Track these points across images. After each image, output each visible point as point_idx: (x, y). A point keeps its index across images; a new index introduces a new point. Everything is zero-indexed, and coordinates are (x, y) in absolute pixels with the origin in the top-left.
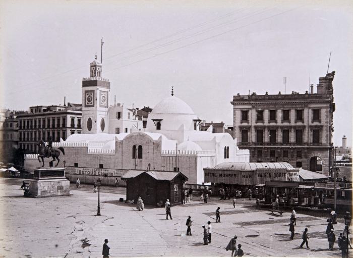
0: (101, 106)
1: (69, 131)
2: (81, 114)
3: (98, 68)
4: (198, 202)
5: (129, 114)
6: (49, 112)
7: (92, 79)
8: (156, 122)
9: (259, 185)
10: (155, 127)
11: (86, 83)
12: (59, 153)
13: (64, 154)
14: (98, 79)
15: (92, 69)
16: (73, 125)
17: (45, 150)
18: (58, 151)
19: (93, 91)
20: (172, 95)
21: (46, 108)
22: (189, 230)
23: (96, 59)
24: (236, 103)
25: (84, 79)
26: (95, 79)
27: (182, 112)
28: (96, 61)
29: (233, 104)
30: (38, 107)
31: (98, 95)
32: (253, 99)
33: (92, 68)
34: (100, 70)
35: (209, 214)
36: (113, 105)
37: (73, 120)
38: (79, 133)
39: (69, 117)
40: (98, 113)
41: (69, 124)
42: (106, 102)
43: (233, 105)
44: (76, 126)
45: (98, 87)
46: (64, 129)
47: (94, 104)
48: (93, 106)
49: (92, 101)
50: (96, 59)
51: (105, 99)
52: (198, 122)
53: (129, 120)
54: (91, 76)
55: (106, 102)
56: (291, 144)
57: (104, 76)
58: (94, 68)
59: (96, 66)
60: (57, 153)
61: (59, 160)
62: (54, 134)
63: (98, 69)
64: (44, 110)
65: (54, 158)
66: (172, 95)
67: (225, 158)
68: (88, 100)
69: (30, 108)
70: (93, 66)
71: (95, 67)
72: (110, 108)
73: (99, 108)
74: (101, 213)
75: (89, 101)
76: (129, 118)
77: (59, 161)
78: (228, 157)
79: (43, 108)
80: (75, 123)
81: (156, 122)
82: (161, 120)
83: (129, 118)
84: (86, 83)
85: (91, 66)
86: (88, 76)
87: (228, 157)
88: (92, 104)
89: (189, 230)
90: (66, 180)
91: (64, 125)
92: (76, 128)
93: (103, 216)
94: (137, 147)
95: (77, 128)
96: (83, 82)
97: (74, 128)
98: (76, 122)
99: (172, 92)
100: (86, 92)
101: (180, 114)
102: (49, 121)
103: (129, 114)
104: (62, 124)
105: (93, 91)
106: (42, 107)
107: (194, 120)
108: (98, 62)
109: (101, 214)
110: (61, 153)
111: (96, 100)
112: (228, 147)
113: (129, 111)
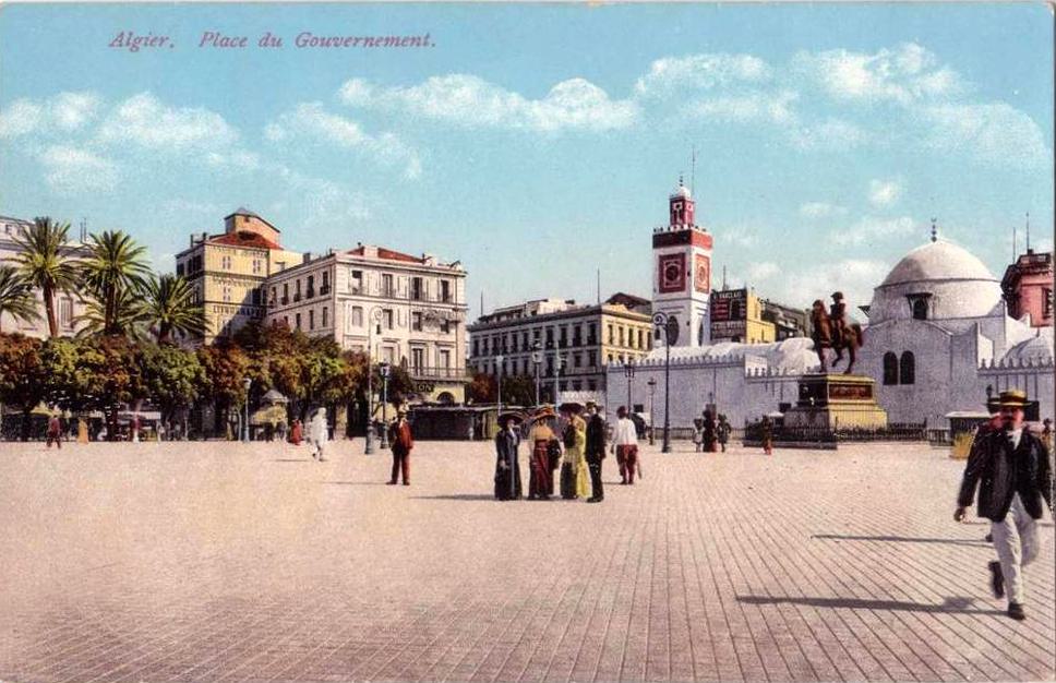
0: (699, 289)
4: (645, 316)
11: (660, 240)
19: (682, 256)
22: (415, 41)
31: (694, 265)
32: (515, 499)
33: (675, 205)
39: (605, 319)
47: (684, 284)
48: (682, 288)
54: (674, 222)
56: (1021, 373)
57: (700, 222)
58: (678, 207)
65: (839, 352)
68: (668, 277)
69: (227, 219)
70: (676, 201)
71: (681, 203)
75: (670, 278)
84: (660, 240)
86: (664, 222)
89: (415, 41)
96: (655, 237)
100: (662, 258)
101: (951, 280)
104: (574, 340)
111: (689, 274)
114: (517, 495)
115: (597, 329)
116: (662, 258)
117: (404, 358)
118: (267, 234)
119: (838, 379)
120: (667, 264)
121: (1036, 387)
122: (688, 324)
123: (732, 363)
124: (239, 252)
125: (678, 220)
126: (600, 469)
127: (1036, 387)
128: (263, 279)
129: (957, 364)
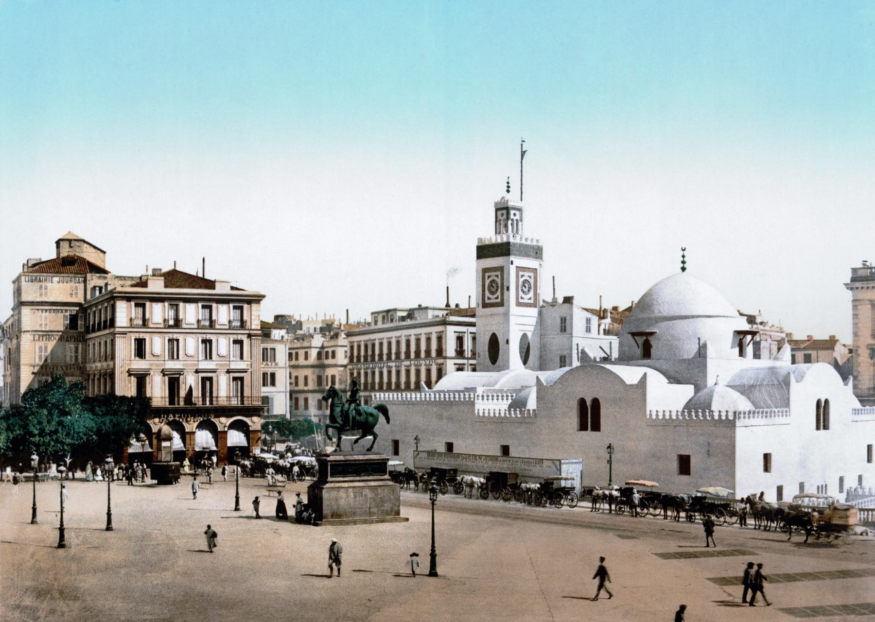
0: (519, 304)
1: (450, 365)
2: (473, 325)
3: (512, 212)
5: (588, 321)
6: (409, 322)
7: (499, 241)
8: (641, 340)
9: (837, 523)
10: (639, 352)
11: (484, 251)
12: (376, 419)
13: (388, 422)
14: (512, 240)
15: (499, 217)
16: (460, 353)
17: (342, 411)
18: (371, 415)
19: (501, 269)
20: (683, 269)
21: (405, 314)
23: (508, 191)
24: (858, 284)
25: (480, 240)
26: (505, 240)
27: (694, 314)
28: (508, 197)
29: (851, 289)
30: (388, 311)
33: (499, 213)
34: (518, 217)
35: (723, 581)
36: (550, 300)
37: (460, 340)
38: (474, 370)
39: (451, 333)
40: (513, 320)
41: (450, 348)
42: (531, 294)
43: (850, 292)
44: (468, 353)
45: (512, 258)
46: (440, 361)
47: (502, 300)
48: (501, 304)
49: (499, 293)
50: (508, 191)
51: (528, 286)
52: (749, 337)
53: (587, 335)
55: (531, 294)
59: (507, 209)
60: (371, 419)
61: (375, 436)
62: (359, 374)
63: (512, 216)
64: (403, 319)
66: (683, 269)
67: (818, 428)
68: (489, 290)
69: (373, 313)
71: (504, 212)
72: (543, 307)
73: (514, 309)
74: (439, 570)
76: (588, 330)
77: (375, 438)
78: (826, 427)
79: (400, 314)
80: (465, 347)
81: (641, 340)
82: (652, 334)
83: (588, 330)
84: (484, 251)
85: (497, 210)
86: (490, 236)
87: (826, 427)
88: (499, 300)
90: (391, 483)
91: (440, 352)
92: (468, 359)
93: (444, 577)
94: (589, 403)
95: (470, 359)
97: (464, 358)
98: (468, 345)
99: (683, 262)
100: (485, 271)
102: (429, 340)
103: (588, 321)
105: (501, 269)
106: (395, 310)
107: (738, 333)
108: (513, 200)
109: (439, 573)
110: (382, 419)
111: (508, 289)
112: (827, 401)
113: (589, 315)
114: (586, 429)
115: (444, 341)
116: (485, 271)
117: (191, 388)
118: (91, 256)
119: (361, 457)
120: (489, 277)
121: (576, 463)
122: (507, 342)
123: (304, 430)
124: (56, 279)
125: (503, 230)
126: (258, 507)
127: (576, 463)
128: (79, 305)
129: (45, 550)
